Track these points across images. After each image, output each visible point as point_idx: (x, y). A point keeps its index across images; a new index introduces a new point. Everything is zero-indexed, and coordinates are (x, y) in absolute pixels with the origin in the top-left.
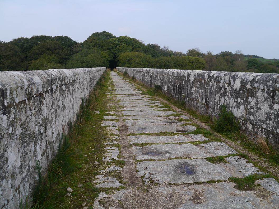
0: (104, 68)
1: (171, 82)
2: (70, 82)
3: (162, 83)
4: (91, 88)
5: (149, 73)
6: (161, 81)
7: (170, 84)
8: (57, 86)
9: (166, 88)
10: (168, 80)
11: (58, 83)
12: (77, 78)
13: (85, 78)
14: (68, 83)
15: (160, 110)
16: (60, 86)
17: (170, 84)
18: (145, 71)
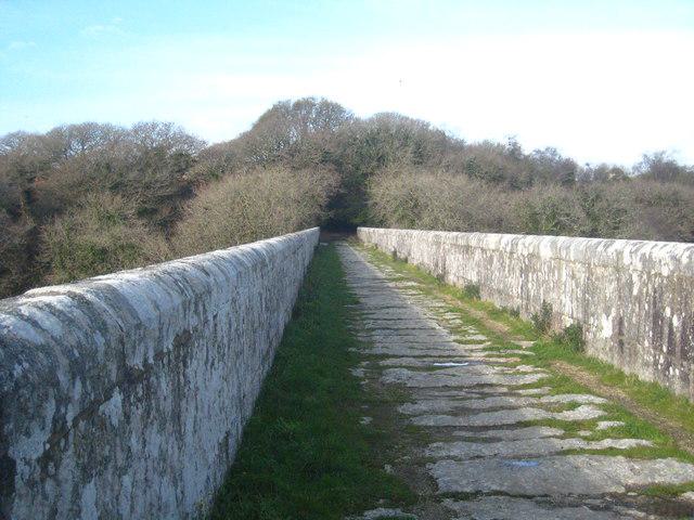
0: (312, 234)
1: (638, 299)
2: (159, 355)
3: (585, 305)
4: (268, 337)
5: (511, 253)
6: (580, 295)
7: (633, 311)
8: (59, 420)
9: (611, 326)
10: (619, 290)
11: (63, 401)
12: (205, 311)
13: (242, 299)
14: (151, 361)
15: (611, 452)
16: (81, 414)
17: (633, 311)
18: (492, 247)
